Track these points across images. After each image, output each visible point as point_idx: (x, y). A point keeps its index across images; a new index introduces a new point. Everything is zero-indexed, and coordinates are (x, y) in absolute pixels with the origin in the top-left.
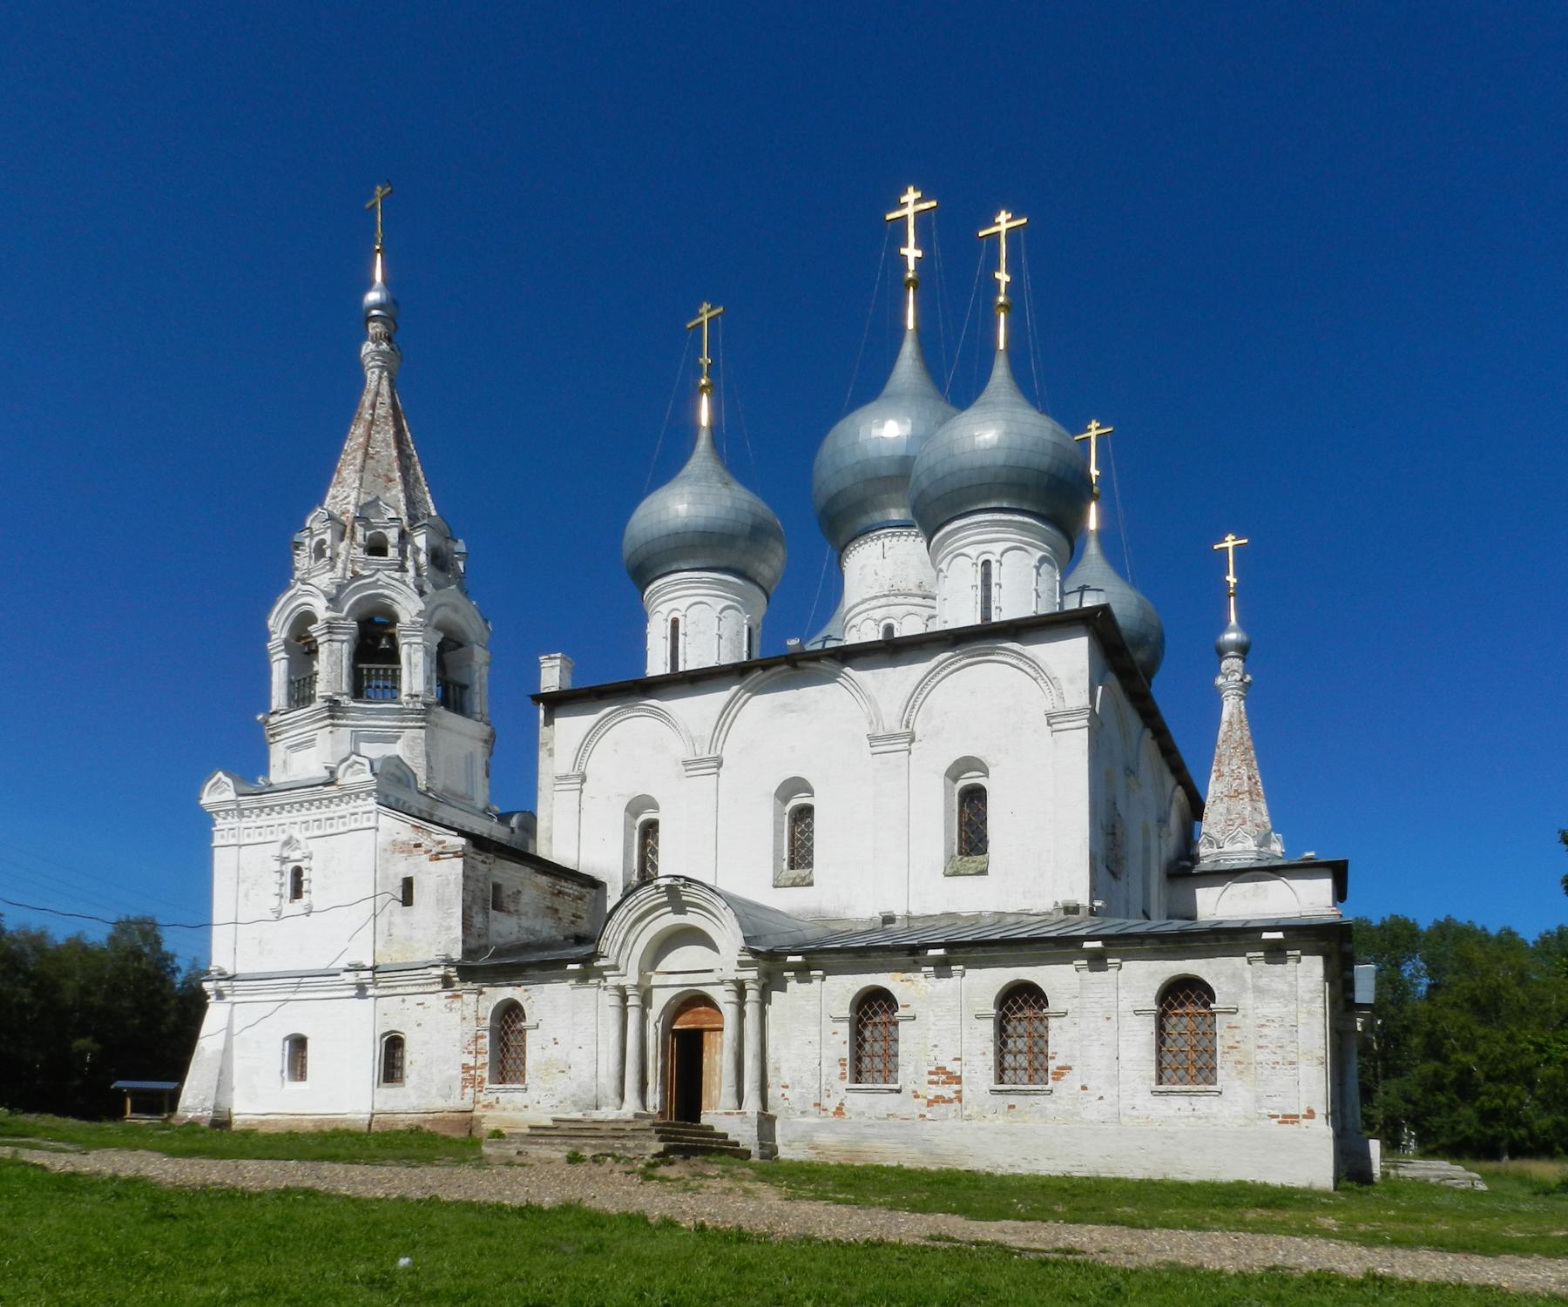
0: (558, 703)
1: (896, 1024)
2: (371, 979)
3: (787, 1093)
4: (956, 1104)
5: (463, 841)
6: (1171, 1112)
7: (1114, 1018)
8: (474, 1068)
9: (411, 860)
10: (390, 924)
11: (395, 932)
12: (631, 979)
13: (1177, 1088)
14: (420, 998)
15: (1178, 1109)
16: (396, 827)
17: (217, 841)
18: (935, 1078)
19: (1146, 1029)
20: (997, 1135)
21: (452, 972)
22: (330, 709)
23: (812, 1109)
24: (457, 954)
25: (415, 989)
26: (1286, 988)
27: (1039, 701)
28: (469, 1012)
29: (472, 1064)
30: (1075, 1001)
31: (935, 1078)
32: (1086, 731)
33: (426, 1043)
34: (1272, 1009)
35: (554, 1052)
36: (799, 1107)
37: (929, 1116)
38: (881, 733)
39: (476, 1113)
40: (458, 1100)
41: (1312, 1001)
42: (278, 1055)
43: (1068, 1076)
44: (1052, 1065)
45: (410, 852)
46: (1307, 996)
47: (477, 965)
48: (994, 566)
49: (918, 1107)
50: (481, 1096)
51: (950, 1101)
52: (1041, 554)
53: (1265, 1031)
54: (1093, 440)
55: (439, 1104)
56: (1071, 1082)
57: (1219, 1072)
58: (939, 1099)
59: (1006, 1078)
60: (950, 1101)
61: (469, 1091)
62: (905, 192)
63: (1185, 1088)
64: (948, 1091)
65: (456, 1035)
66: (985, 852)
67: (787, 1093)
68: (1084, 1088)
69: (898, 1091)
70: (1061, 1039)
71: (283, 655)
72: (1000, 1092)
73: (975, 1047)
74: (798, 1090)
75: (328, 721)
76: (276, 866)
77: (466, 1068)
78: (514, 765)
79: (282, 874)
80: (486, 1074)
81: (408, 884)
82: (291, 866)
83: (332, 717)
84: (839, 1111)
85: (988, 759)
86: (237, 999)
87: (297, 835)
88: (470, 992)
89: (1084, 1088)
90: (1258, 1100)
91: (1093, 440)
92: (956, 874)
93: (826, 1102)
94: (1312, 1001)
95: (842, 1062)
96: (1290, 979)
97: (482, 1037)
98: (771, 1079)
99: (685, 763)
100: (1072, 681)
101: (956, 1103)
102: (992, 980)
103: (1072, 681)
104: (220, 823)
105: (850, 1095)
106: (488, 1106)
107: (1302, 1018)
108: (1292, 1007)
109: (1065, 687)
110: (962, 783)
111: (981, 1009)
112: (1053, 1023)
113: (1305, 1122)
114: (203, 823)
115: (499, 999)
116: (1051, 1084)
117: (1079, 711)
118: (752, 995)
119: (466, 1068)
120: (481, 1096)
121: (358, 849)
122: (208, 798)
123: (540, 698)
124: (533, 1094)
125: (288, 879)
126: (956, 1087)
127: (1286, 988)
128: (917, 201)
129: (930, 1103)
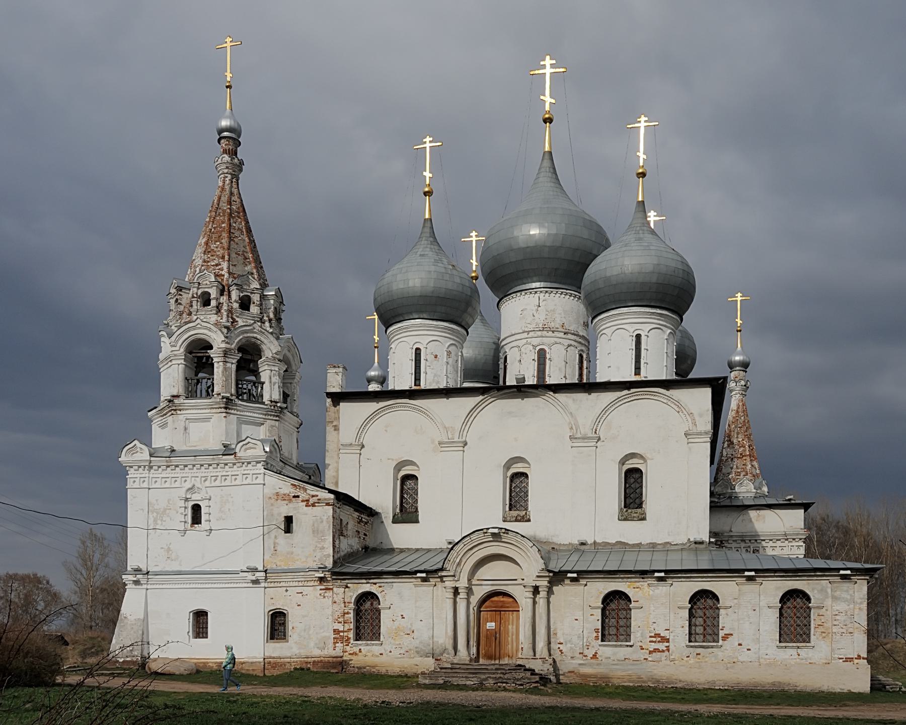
0: (337, 398)
1: (630, 610)
2: (263, 576)
3: (561, 647)
4: (667, 653)
5: (332, 496)
6: (787, 657)
7: (757, 609)
8: (343, 632)
9: (291, 505)
10: (275, 543)
11: (278, 548)
12: (463, 583)
13: (791, 644)
14: (299, 589)
15: (790, 654)
16: (285, 486)
17: (130, 484)
18: (654, 639)
19: (773, 617)
20: (618, 662)
21: (328, 575)
22: (227, 403)
23: (578, 655)
24: (329, 563)
25: (297, 584)
26: (849, 597)
27: (682, 425)
28: (339, 598)
29: (341, 629)
30: (736, 601)
31: (654, 639)
32: (709, 444)
33: (304, 616)
34: (841, 606)
35: (400, 622)
36: (570, 655)
37: (650, 659)
38: (579, 435)
39: (345, 658)
40: (331, 651)
41: (861, 603)
42: (186, 624)
43: (731, 638)
44: (721, 633)
45: (290, 501)
46: (859, 601)
47: (341, 570)
48: (643, 339)
49: (644, 654)
50: (348, 648)
51: (663, 651)
52: (669, 331)
53: (837, 617)
54: (428, 150)
55: (317, 652)
56: (733, 642)
57: (812, 637)
58: (656, 650)
59: (693, 640)
60: (663, 651)
61: (339, 645)
62: (544, 60)
63: (794, 644)
64: (662, 646)
65: (329, 612)
66: (640, 506)
67: (561, 647)
68: (740, 645)
69: (631, 646)
70: (726, 620)
71: (182, 361)
72: (692, 647)
73: (677, 624)
74: (569, 645)
75: (223, 410)
76: (182, 504)
77: (336, 631)
78: (314, 436)
79: (186, 508)
80: (351, 635)
81: (289, 520)
82: (191, 504)
83: (226, 408)
84: (595, 656)
85: (647, 455)
86: (149, 587)
87: (198, 485)
88: (340, 587)
89: (740, 645)
90: (832, 650)
91: (428, 150)
92: (625, 519)
93: (586, 652)
94: (861, 603)
95: (597, 631)
96: (851, 592)
97: (348, 613)
98: (552, 640)
99: (440, 443)
100: (701, 415)
101: (667, 653)
102: (688, 588)
103: (701, 415)
104: (131, 472)
105: (601, 648)
106: (355, 654)
107: (857, 611)
108: (852, 606)
109: (697, 418)
110: (626, 467)
111: (680, 604)
112: (722, 612)
113: (856, 661)
114: (121, 473)
115: (360, 591)
116: (721, 641)
117: (706, 433)
118: (543, 594)
119: (336, 631)
120: (348, 648)
121: (247, 495)
122: (124, 458)
123: (330, 395)
124: (387, 647)
125: (189, 512)
126: (667, 644)
127: (849, 597)
128: (552, 66)
129: (651, 652)
